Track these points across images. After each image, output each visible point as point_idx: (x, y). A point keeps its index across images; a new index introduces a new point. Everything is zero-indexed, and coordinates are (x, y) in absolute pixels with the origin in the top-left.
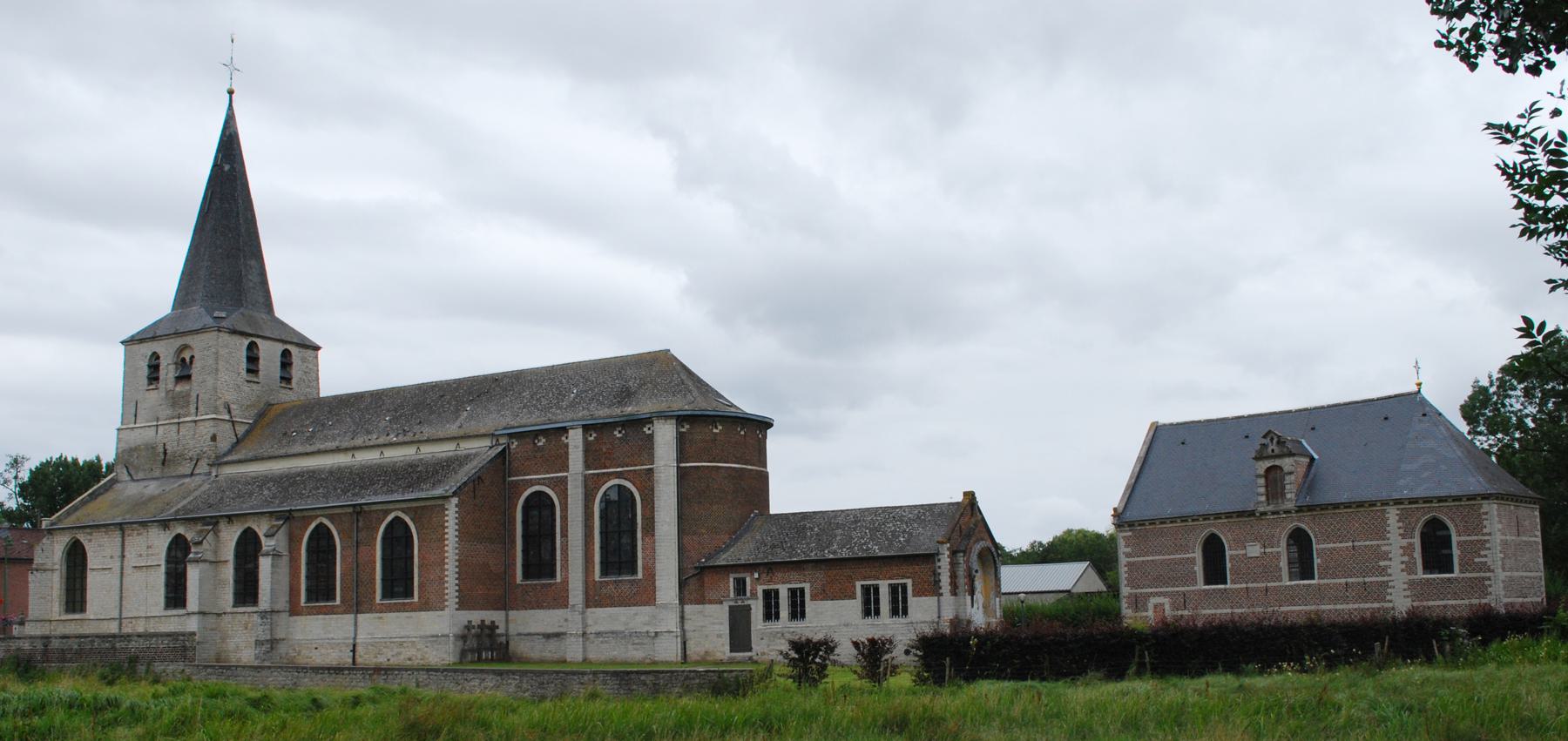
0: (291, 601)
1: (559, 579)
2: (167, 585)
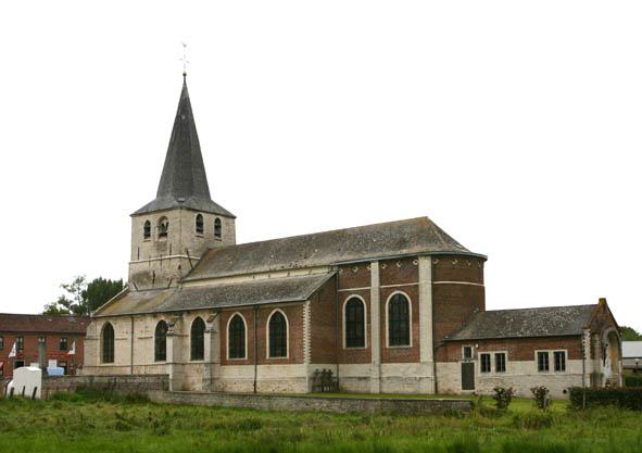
1: (366, 347)
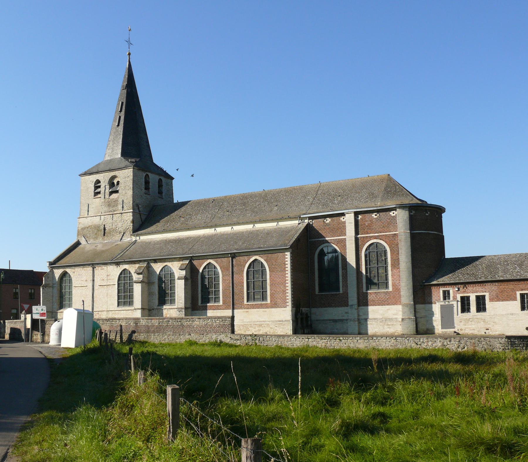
1: (341, 292)
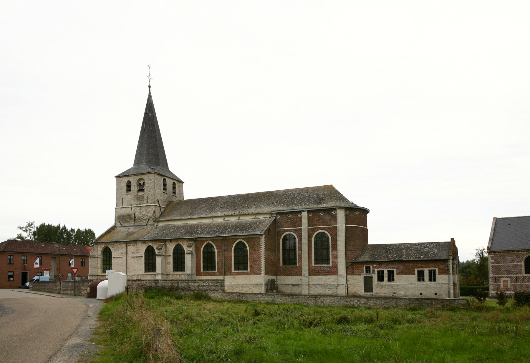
0: (197, 270)
1: (298, 265)
2: (145, 264)
